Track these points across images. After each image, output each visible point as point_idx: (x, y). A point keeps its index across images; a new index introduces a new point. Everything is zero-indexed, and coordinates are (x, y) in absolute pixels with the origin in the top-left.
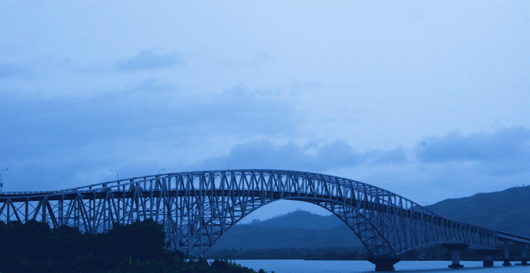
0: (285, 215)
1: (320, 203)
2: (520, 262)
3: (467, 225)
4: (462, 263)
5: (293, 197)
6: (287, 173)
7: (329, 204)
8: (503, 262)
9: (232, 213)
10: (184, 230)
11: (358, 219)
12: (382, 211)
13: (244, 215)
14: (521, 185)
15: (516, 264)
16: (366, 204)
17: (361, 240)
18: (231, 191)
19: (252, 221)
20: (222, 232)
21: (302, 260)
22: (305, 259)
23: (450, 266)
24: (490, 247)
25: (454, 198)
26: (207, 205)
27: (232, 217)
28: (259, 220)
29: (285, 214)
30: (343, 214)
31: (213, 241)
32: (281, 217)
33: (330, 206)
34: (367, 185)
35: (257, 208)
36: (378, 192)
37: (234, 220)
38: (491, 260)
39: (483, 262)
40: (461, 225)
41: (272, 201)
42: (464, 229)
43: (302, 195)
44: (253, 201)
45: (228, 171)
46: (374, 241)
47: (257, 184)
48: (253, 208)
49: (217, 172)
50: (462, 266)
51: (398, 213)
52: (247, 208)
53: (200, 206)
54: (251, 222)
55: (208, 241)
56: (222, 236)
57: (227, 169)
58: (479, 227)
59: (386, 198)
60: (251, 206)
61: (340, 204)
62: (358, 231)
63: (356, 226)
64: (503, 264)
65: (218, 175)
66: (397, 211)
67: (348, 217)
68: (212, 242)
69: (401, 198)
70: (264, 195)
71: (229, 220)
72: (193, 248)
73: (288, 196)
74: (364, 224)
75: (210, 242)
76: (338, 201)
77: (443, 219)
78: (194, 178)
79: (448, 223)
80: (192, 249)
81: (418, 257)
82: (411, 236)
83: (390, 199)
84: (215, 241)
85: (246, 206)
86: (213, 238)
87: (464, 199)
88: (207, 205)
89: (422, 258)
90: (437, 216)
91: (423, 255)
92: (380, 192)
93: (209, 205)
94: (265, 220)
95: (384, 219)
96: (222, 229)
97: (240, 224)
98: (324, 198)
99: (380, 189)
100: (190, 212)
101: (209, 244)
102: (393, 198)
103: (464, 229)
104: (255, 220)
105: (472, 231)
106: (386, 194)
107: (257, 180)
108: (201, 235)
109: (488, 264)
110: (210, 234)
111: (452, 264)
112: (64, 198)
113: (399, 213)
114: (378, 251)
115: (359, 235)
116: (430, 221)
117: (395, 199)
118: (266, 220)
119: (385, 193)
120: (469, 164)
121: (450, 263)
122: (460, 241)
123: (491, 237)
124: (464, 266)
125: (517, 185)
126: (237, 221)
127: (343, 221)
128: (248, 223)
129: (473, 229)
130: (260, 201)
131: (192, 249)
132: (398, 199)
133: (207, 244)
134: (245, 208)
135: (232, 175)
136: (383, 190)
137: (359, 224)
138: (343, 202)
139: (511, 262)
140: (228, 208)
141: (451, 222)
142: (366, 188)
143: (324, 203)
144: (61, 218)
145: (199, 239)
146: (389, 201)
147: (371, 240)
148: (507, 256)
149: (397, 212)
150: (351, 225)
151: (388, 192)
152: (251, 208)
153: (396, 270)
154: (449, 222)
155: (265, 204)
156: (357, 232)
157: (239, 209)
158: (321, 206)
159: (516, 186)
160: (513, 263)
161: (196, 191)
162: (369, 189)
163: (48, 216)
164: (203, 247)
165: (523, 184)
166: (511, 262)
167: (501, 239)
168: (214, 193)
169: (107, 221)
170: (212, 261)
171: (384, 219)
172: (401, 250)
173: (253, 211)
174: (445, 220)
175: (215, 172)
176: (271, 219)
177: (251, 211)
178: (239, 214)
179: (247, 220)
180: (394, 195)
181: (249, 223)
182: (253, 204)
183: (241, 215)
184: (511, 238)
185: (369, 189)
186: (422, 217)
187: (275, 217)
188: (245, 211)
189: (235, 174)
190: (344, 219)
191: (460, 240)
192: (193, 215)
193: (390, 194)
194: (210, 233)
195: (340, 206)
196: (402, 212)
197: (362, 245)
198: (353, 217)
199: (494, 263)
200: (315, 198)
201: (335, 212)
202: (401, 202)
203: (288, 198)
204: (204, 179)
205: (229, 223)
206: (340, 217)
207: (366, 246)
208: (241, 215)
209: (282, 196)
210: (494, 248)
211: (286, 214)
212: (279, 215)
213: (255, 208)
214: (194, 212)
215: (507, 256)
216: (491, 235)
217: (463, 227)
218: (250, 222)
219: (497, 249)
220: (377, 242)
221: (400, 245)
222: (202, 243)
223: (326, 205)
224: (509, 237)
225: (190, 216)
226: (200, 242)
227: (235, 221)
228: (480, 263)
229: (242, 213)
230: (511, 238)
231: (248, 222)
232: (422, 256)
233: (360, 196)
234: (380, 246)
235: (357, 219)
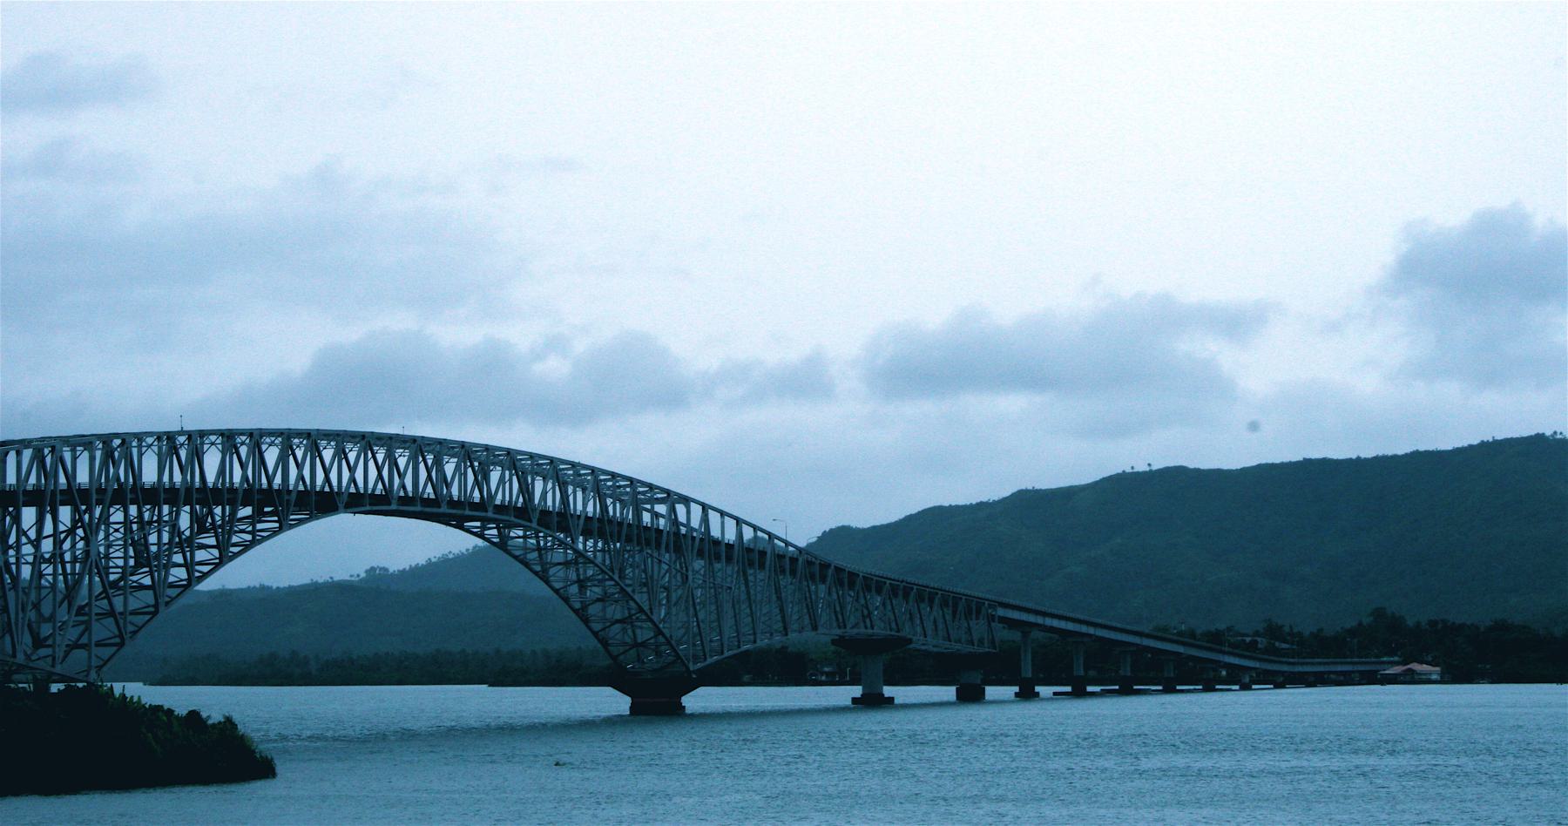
0: (463, 553)
1: (465, 524)
2: (1068, 689)
3: (904, 584)
4: (888, 691)
5: (375, 508)
6: (357, 440)
7: (494, 526)
8: (1017, 689)
9: (188, 554)
10: (45, 597)
11: (581, 571)
12: (648, 544)
13: (225, 559)
14: (1141, 467)
15: (1055, 694)
16: (599, 527)
17: (590, 629)
18: (52, 491)
19: (366, 571)
20: (156, 606)
21: (484, 687)
22: (492, 685)
23: (855, 700)
24: (973, 645)
25: (953, 504)
26: (117, 530)
27: (189, 565)
28: (386, 570)
29: (464, 551)
30: (535, 554)
31: (131, 633)
32: (452, 559)
33: (495, 532)
34: (605, 472)
35: (265, 539)
36: (637, 492)
37: (193, 575)
38: (979, 682)
39: (957, 690)
40: (888, 585)
41: (311, 518)
42: (896, 595)
43: (406, 500)
44: (258, 516)
45: (181, 433)
46: (630, 632)
47: (327, 472)
48: (254, 538)
49: (211, 434)
50: (891, 700)
51: (695, 551)
52: (235, 539)
53: (91, 533)
54: (363, 575)
55: (117, 632)
56: (159, 616)
57: (180, 429)
58: (941, 590)
59: (661, 509)
61: (526, 528)
62: (581, 602)
63: (574, 589)
64: (1017, 695)
65: (213, 444)
66: (693, 545)
67: (550, 563)
68: (125, 637)
69: (705, 508)
70: (288, 501)
71: (179, 574)
72: (67, 654)
73: (361, 502)
74: (596, 582)
75: (121, 636)
76: (513, 519)
77: (833, 565)
78: (78, 453)
79: (846, 579)
80: (63, 661)
81: (812, 675)
82: (735, 616)
83: (673, 510)
84: (135, 633)
85: (231, 533)
86: (130, 623)
87: (981, 506)
88: (117, 530)
89: (824, 678)
90: (813, 560)
91: (826, 669)
92: (643, 493)
93: (122, 530)
94: (404, 569)
95: (652, 567)
96: (156, 599)
97: (330, 580)
98: (470, 510)
99: (644, 484)
100: (66, 551)
101: (117, 640)
102: (680, 509)
103: (896, 595)
104: (373, 569)
105: (920, 598)
106: (662, 498)
107: (327, 462)
108: (94, 617)
109: (970, 695)
110: (121, 614)
111: (862, 695)
112: (131, 499)
113: (699, 550)
114: (639, 659)
115: (582, 614)
116: (793, 573)
117: (688, 512)
118: (408, 568)
119: (659, 496)
120: (1013, 404)
121: (857, 691)
122: (762, 633)
123: (977, 618)
124: (896, 701)
125: (1133, 468)
126: (205, 575)
127: (536, 573)
128: (353, 579)
129: (926, 596)
130: (276, 518)
131: (63, 661)
132: (696, 510)
133: (113, 641)
134: (230, 538)
135: (188, 445)
136: (651, 487)
137: (582, 584)
138: (531, 521)
139: (1037, 689)
140: (177, 540)
141: (845, 570)
142: (597, 481)
143: (478, 524)
144: (680, 558)
145: (88, 629)
146: (670, 516)
147: (618, 626)
148: (1027, 671)
149: (692, 550)
150: (557, 585)
151: (668, 492)
152: (249, 537)
153: (688, 711)
154: (853, 576)
155: (291, 527)
156: (578, 606)
157: (213, 541)
158: (468, 531)
159: (1128, 470)
160: (1044, 691)
162: (610, 483)
163: (119, 560)
164: (95, 650)
165: (1149, 465)
166: (1037, 689)
167: (1011, 624)
168: (133, 496)
169: (627, 572)
170: (61, 686)
171: (652, 567)
172: (705, 655)
173: (252, 548)
174: (838, 570)
175: (203, 434)
176: (422, 565)
177: (247, 547)
178: (213, 557)
179: (245, 573)
180: (686, 501)
181: (357, 579)
182: (254, 527)
183: (217, 559)
184: (1040, 620)
185: (610, 483)
186: (768, 563)
187: (433, 560)
188: (228, 548)
189: (263, 443)
190: (538, 568)
191: (785, 628)
192: (74, 560)
193: (672, 498)
194: (121, 610)
195: (525, 531)
196: (712, 548)
197: (593, 643)
198: (566, 564)
199: (987, 693)
200: (444, 509)
201: (509, 548)
202: (705, 520)
203: (363, 509)
204: (174, 450)
205: (182, 580)
206: (526, 564)
207: (605, 643)
208: (217, 559)
209: (341, 506)
210: (987, 650)
211: (467, 550)
212: (446, 552)
213: (258, 538)
214: (79, 549)
215: (1027, 671)
216: (978, 612)
217: (894, 591)
218: (358, 576)
219: (994, 651)
220: (638, 632)
221: (721, 638)
222: (95, 639)
223: (484, 528)
224: (1031, 618)
225: (68, 562)
226: (90, 634)
227: (197, 574)
228: (949, 693)
229: (220, 554)
230: (1040, 620)
231: (351, 576)
232: (822, 673)
233: (582, 504)
234: (643, 644)
235: (577, 570)
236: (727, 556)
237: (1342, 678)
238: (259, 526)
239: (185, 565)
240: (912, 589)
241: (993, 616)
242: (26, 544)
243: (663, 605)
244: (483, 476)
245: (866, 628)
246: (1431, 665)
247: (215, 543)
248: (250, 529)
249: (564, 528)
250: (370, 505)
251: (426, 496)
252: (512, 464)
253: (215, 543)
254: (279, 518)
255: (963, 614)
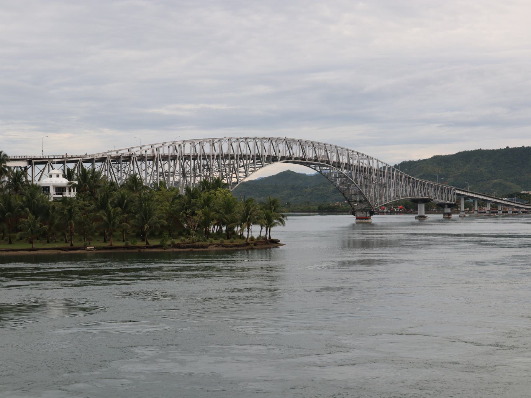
33: (319, 168)
48: (255, 169)
60: (253, 168)
102: (371, 161)
117: (373, 162)
130: (261, 164)
143: (314, 165)
152: (254, 169)
157: (244, 170)
161: (244, 155)
182: (255, 166)
183: (92, 164)
200: (307, 161)
227: (240, 180)
229: (246, 174)
236: (349, 168)
237: (116, 270)
238: (256, 166)
239: (236, 177)
240: (433, 185)
241: (454, 193)
242: (151, 168)
243: (192, 177)
244: (290, 148)
245: (442, 199)
246: (64, 250)
247: (244, 171)
248: (254, 166)
249: (339, 167)
250: (287, 160)
251: (273, 155)
252: (337, 151)
253: (244, 171)
254: (262, 163)
255: (446, 194)
